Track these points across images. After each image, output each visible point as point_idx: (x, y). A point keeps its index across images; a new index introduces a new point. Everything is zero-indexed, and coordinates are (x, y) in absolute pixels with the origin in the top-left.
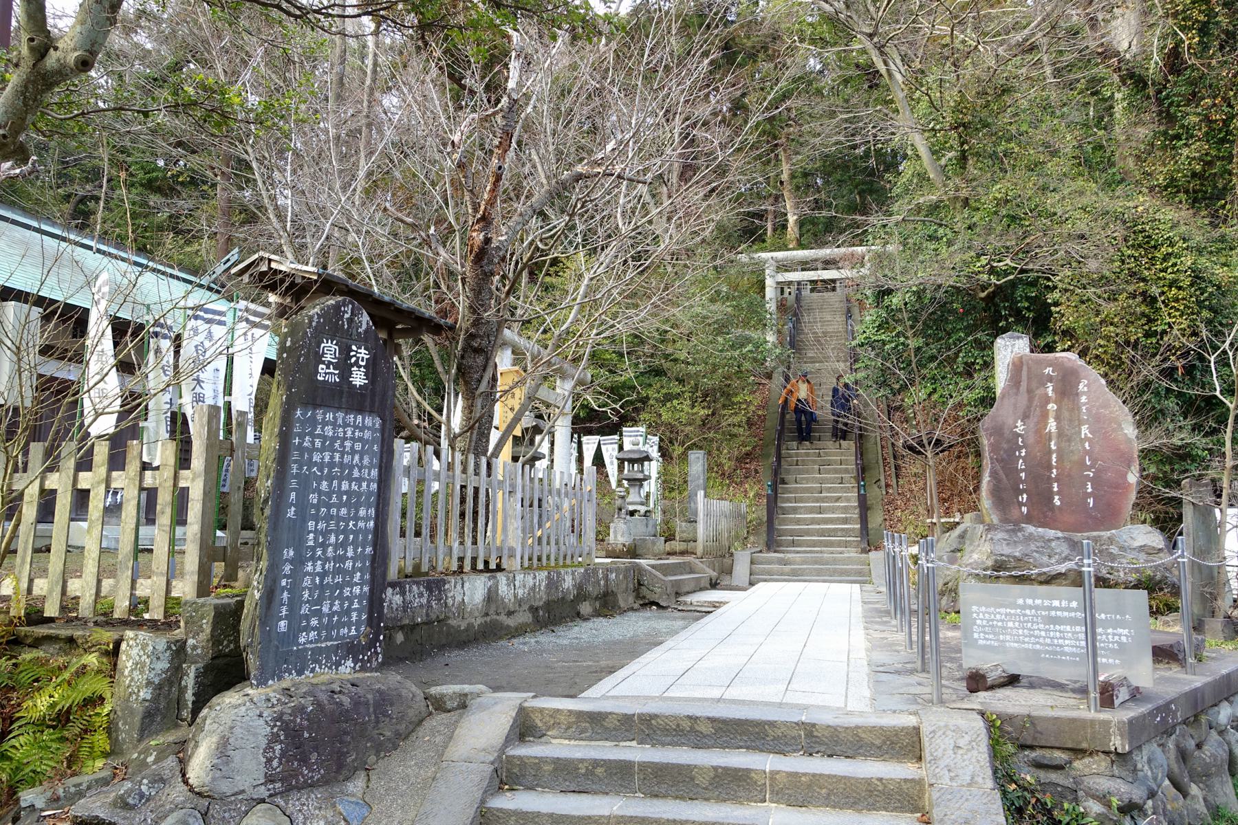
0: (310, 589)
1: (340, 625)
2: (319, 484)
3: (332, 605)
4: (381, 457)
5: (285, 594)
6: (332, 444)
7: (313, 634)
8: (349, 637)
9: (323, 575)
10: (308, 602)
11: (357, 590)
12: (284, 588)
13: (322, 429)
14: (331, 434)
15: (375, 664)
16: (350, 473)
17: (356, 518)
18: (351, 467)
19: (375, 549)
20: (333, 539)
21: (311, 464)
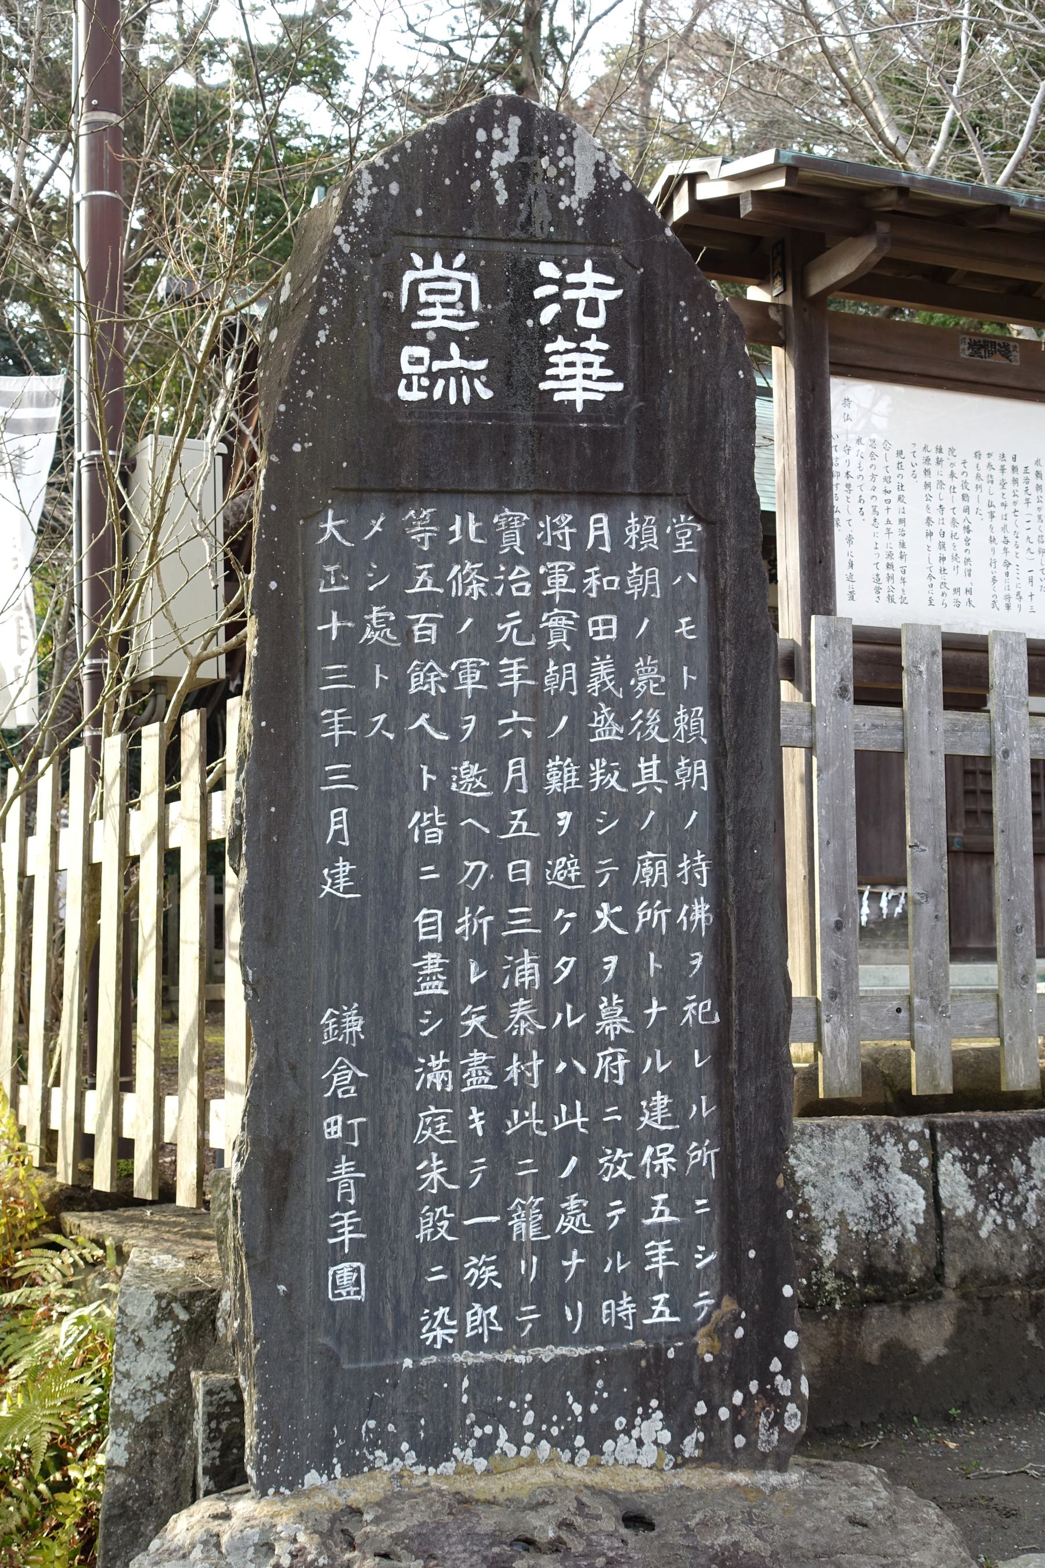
0: (447, 1154)
1: (596, 1286)
2: (445, 777)
3: (550, 1215)
4: (716, 661)
5: (345, 1171)
6: (486, 627)
7: (480, 1317)
8: (640, 1331)
9: (501, 1101)
10: (444, 1197)
11: (661, 1159)
12: (333, 1151)
13: (439, 576)
14: (476, 590)
15: (768, 1439)
16: (580, 728)
17: (627, 894)
18: (583, 708)
19: (723, 1006)
20: (528, 970)
21: (400, 703)
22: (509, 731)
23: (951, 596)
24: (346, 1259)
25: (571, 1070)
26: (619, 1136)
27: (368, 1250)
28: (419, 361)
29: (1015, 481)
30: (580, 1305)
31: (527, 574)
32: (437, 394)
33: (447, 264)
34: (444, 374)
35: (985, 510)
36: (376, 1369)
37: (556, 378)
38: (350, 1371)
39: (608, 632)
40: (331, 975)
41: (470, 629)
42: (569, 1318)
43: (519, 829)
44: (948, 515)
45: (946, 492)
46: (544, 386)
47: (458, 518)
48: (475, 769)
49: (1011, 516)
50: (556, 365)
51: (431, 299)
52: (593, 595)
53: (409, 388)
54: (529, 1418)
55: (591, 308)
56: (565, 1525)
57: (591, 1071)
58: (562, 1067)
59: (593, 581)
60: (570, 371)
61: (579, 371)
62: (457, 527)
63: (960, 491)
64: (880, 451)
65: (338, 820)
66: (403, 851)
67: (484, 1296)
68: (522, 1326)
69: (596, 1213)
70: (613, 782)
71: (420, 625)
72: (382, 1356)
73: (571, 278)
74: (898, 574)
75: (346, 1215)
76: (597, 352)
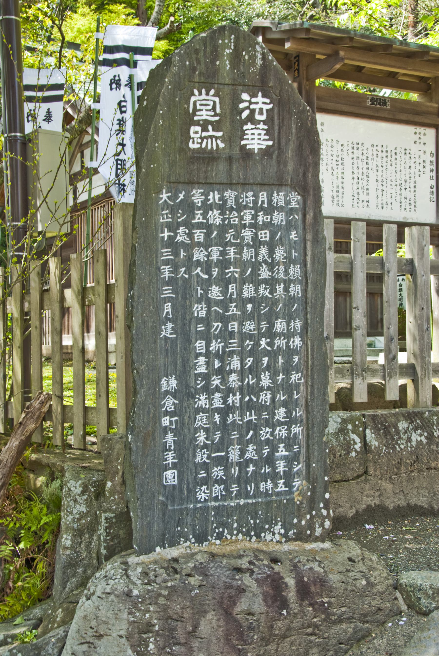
0: (207, 430)
1: (259, 477)
2: (206, 292)
3: (243, 452)
6: (221, 235)
7: (218, 490)
9: (226, 411)
10: (205, 446)
12: (165, 430)
13: (205, 215)
15: (318, 532)
17: (271, 335)
20: (236, 363)
21: (190, 263)
22: (230, 274)
23: (361, 204)
24: (170, 469)
25: (251, 399)
26: (268, 423)
27: (178, 466)
28: (196, 132)
29: (387, 156)
30: (253, 484)
31: (236, 215)
32: (204, 146)
33: (207, 94)
34: (206, 137)
35: (375, 169)
36: (181, 509)
37: (248, 139)
38: (171, 510)
39: (266, 237)
40: (165, 365)
41: (216, 236)
42: (249, 489)
43: (233, 311)
44: (360, 170)
45: (360, 161)
46: (243, 143)
47: (211, 193)
48: (217, 289)
49: (385, 171)
50: (247, 134)
51: (202, 107)
52: (261, 223)
53: (193, 143)
54: (235, 525)
55: (261, 113)
56: (250, 562)
57: (258, 400)
58: (247, 398)
59: (260, 218)
60: (253, 137)
61: (256, 137)
62: (211, 197)
63: (365, 161)
64: (335, 144)
65: (168, 308)
66: (191, 319)
67: (219, 482)
68: (232, 492)
69: (259, 452)
70: (267, 294)
71: (198, 234)
72: (182, 504)
73: (254, 100)
74: (340, 194)
75: (170, 453)
76: (263, 129)
